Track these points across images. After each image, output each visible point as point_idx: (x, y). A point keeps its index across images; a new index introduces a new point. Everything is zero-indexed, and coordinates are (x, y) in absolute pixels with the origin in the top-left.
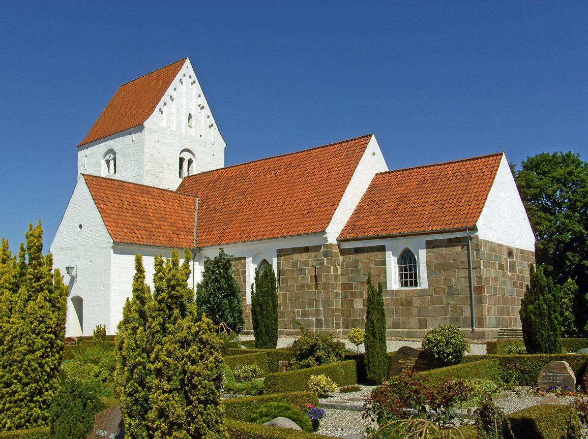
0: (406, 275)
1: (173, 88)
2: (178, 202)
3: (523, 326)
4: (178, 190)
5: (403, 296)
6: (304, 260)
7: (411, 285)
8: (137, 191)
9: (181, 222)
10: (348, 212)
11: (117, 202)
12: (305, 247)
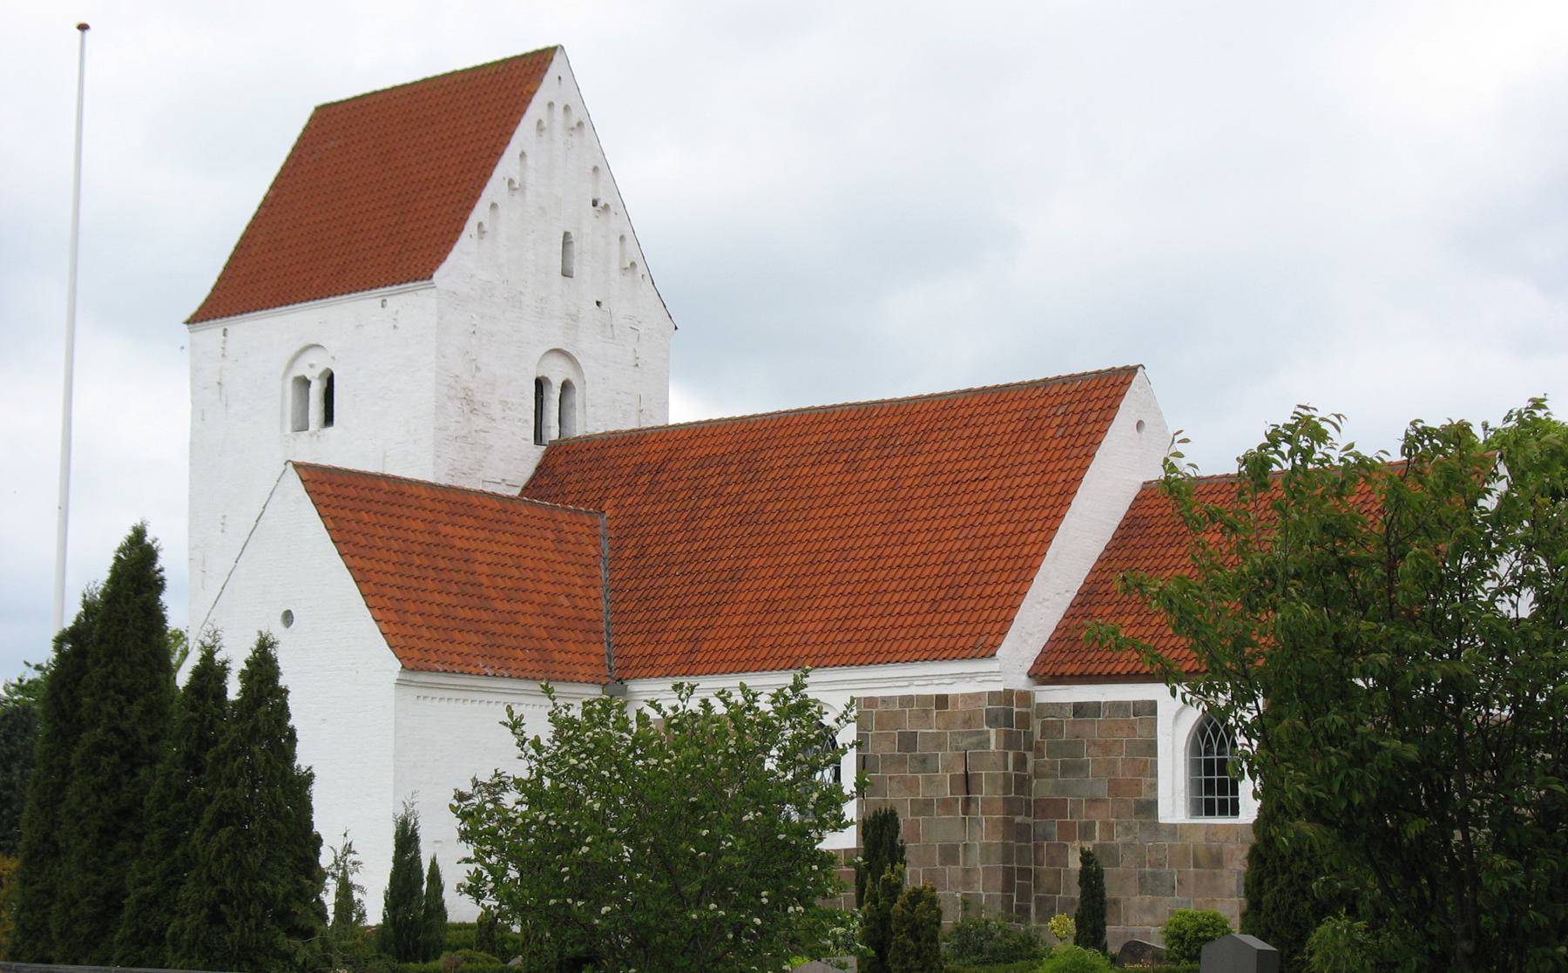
0: (1209, 784)
1: (518, 152)
2: (552, 537)
3: (1083, 894)
4: (531, 488)
5: (1200, 838)
6: (935, 731)
7: (1223, 812)
8: (439, 507)
9: (566, 602)
10: (1068, 595)
11: (395, 546)
12: (937, 696)
